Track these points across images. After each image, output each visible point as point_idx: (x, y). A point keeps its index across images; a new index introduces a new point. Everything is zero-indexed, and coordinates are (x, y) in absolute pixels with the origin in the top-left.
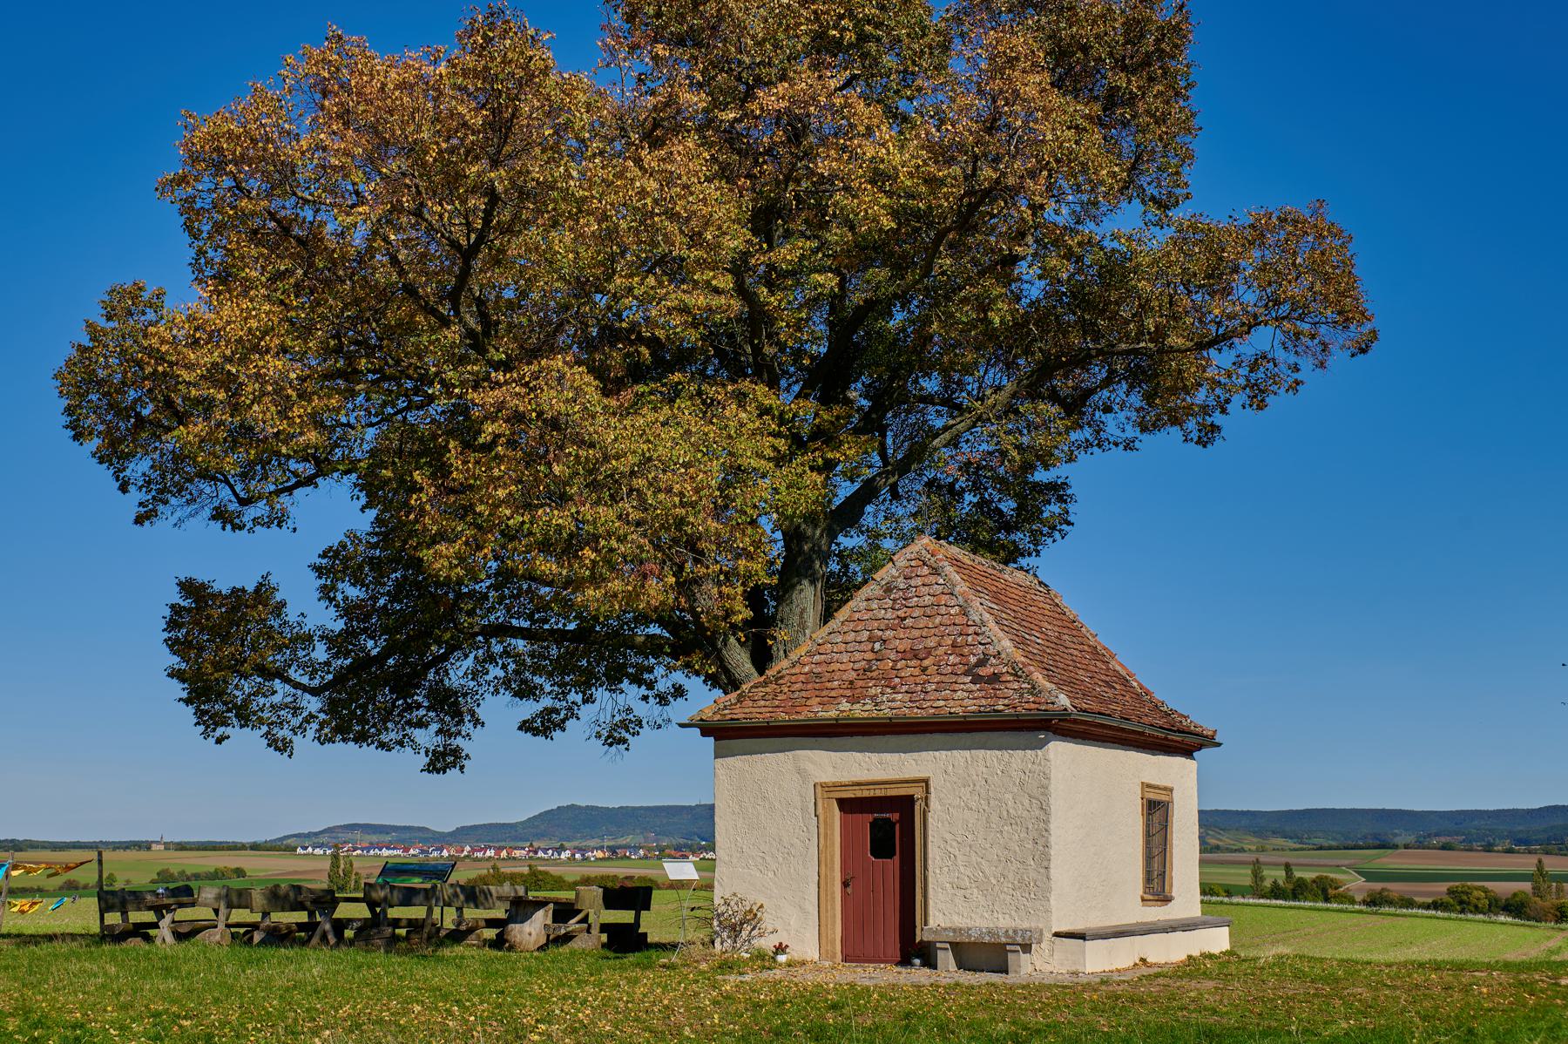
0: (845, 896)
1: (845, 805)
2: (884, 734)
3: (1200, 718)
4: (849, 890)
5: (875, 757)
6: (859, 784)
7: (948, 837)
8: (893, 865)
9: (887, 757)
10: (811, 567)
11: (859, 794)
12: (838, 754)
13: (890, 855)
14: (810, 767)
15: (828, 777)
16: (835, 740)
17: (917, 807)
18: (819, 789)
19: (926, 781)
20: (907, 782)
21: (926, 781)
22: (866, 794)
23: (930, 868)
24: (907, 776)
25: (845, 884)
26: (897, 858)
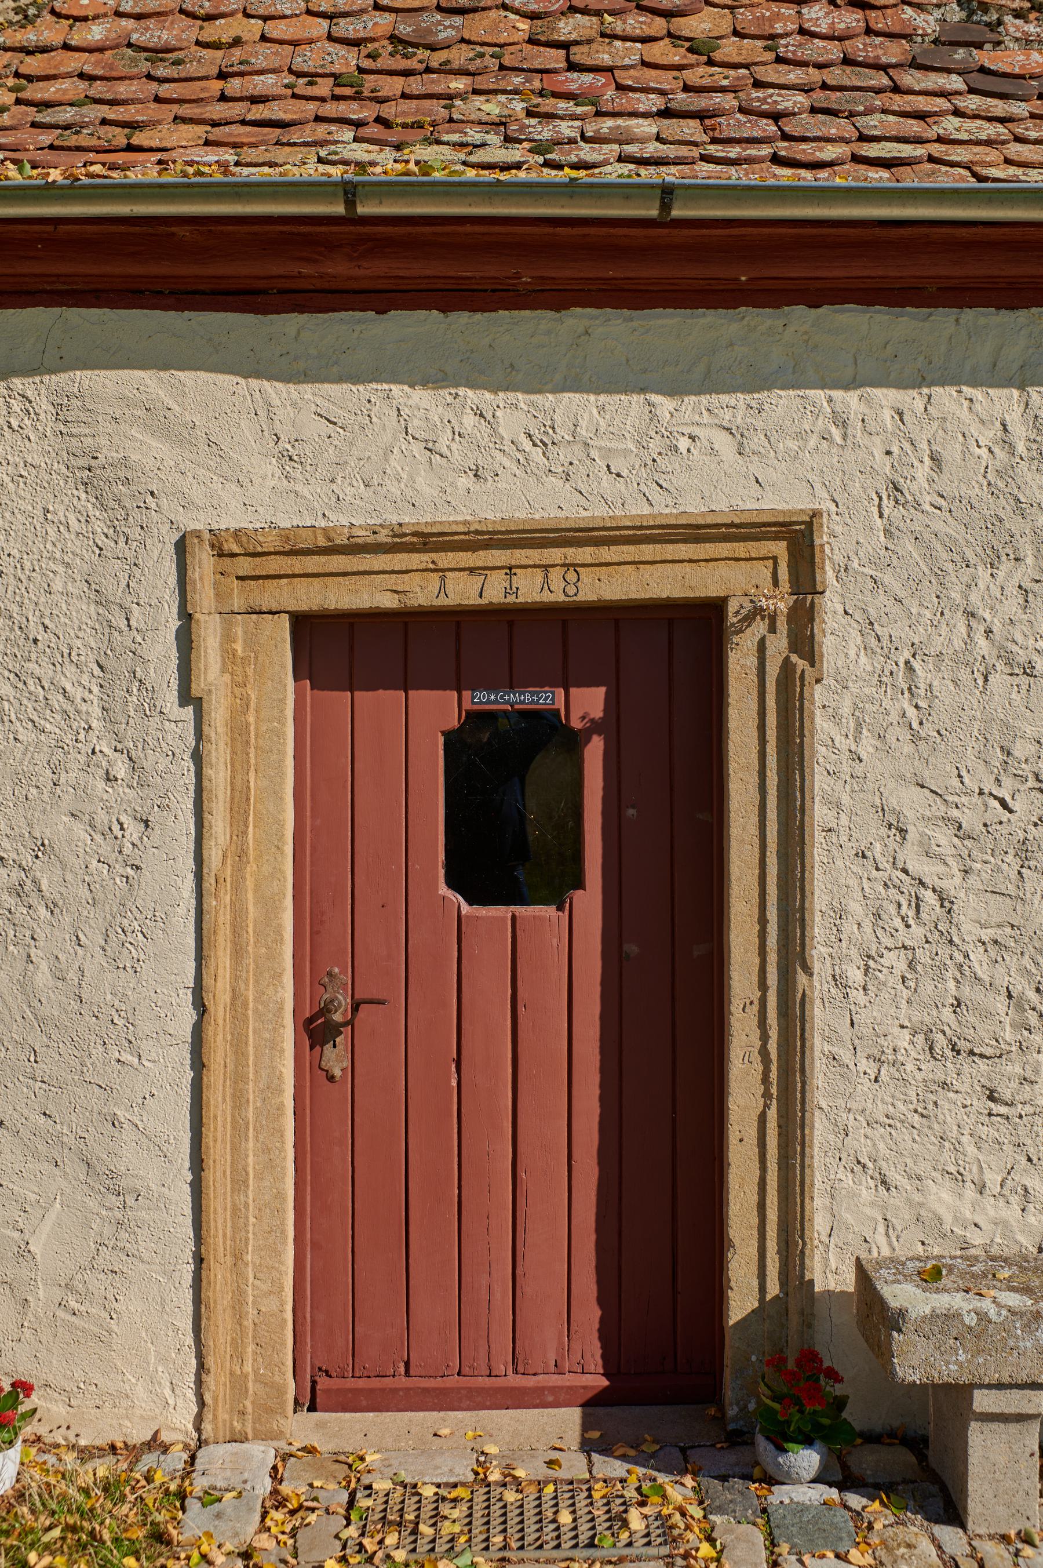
0: (311, 1077)
1: (336, 650)
2: (557, 297)
3: (380, 997)
4: (335, 1058)
5: (514, 413)
6: (427, 541)
7: (910, 802)
8: (566, 938)
9: (577, 409)
10: (819, 1389)
11: (423, 593)
12: (308, 393)
13: (559, 882)
14: (148, 451)
15: (258, 500)
16: (290, 324)
17: (739, 662)
18: (204, 564)
19: (799, 541)
20: (695, 533)
21: (799, 541)
22: (462, 592)
23: (819, 950)
24: (693, 506)
25: (316, 1030)
26: (589, 901)
